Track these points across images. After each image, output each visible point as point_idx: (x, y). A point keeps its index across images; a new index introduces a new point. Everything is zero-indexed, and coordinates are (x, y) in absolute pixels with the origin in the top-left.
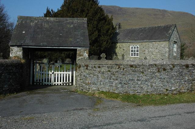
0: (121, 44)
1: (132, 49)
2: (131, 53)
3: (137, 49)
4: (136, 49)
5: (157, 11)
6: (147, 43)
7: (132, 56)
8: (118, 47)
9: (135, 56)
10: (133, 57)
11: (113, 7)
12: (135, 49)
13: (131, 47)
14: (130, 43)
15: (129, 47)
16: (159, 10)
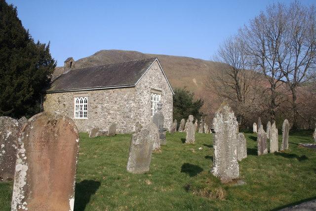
3: (86, 104)
6: (101, 91)
10: (79, 120)
12: (81, 104)
14: (74, 93)
15: (73, 99)
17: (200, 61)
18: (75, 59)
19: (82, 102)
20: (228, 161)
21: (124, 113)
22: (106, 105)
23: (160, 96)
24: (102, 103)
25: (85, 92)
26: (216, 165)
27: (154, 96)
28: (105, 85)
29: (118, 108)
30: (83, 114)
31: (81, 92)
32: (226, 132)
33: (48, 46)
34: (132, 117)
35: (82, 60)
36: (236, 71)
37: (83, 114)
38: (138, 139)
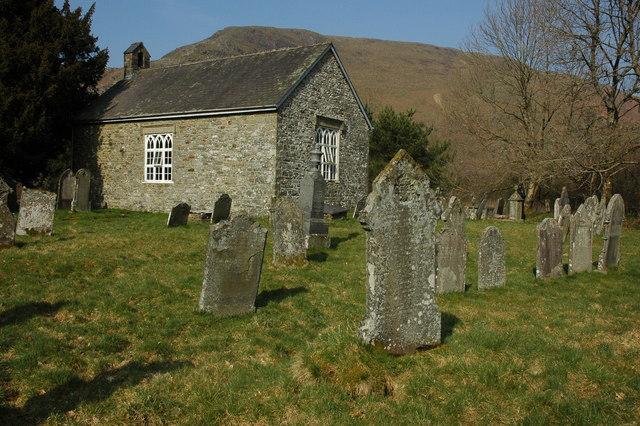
0: (115, 127)
1: (151, 150)
2: (146, 166)
3: (169, 150)
4: (164, 150)
5: (429, 52)
6: (201, 121)
7: (150, 181)
8: (106, 140)
9: (159, 181)
10: (154, 185)
11: (298, 33)
12: (159, 150)
13: (147, 140)
14: (143, 124)
15: (140, 139)
16: (437, 48)
17: (452, 52)
18: (156, 53)
19: (159, 145)
20: (408, 304)
21: (253, 171)
22: (211, 152)
23: (338, 135)
24: (204, 149)
25: (167, 122)
26: (373, 314)
27: (323, 133)
28: (214, 104)
29: (240, 159)
30: (163, 174)
31: (158, 123)
32: (404, 231)
33: (88, 16)
34: (269, 180)
35: (183, 49)
36: (525, 76)
37: (163, 174)
38: (224, 238)
